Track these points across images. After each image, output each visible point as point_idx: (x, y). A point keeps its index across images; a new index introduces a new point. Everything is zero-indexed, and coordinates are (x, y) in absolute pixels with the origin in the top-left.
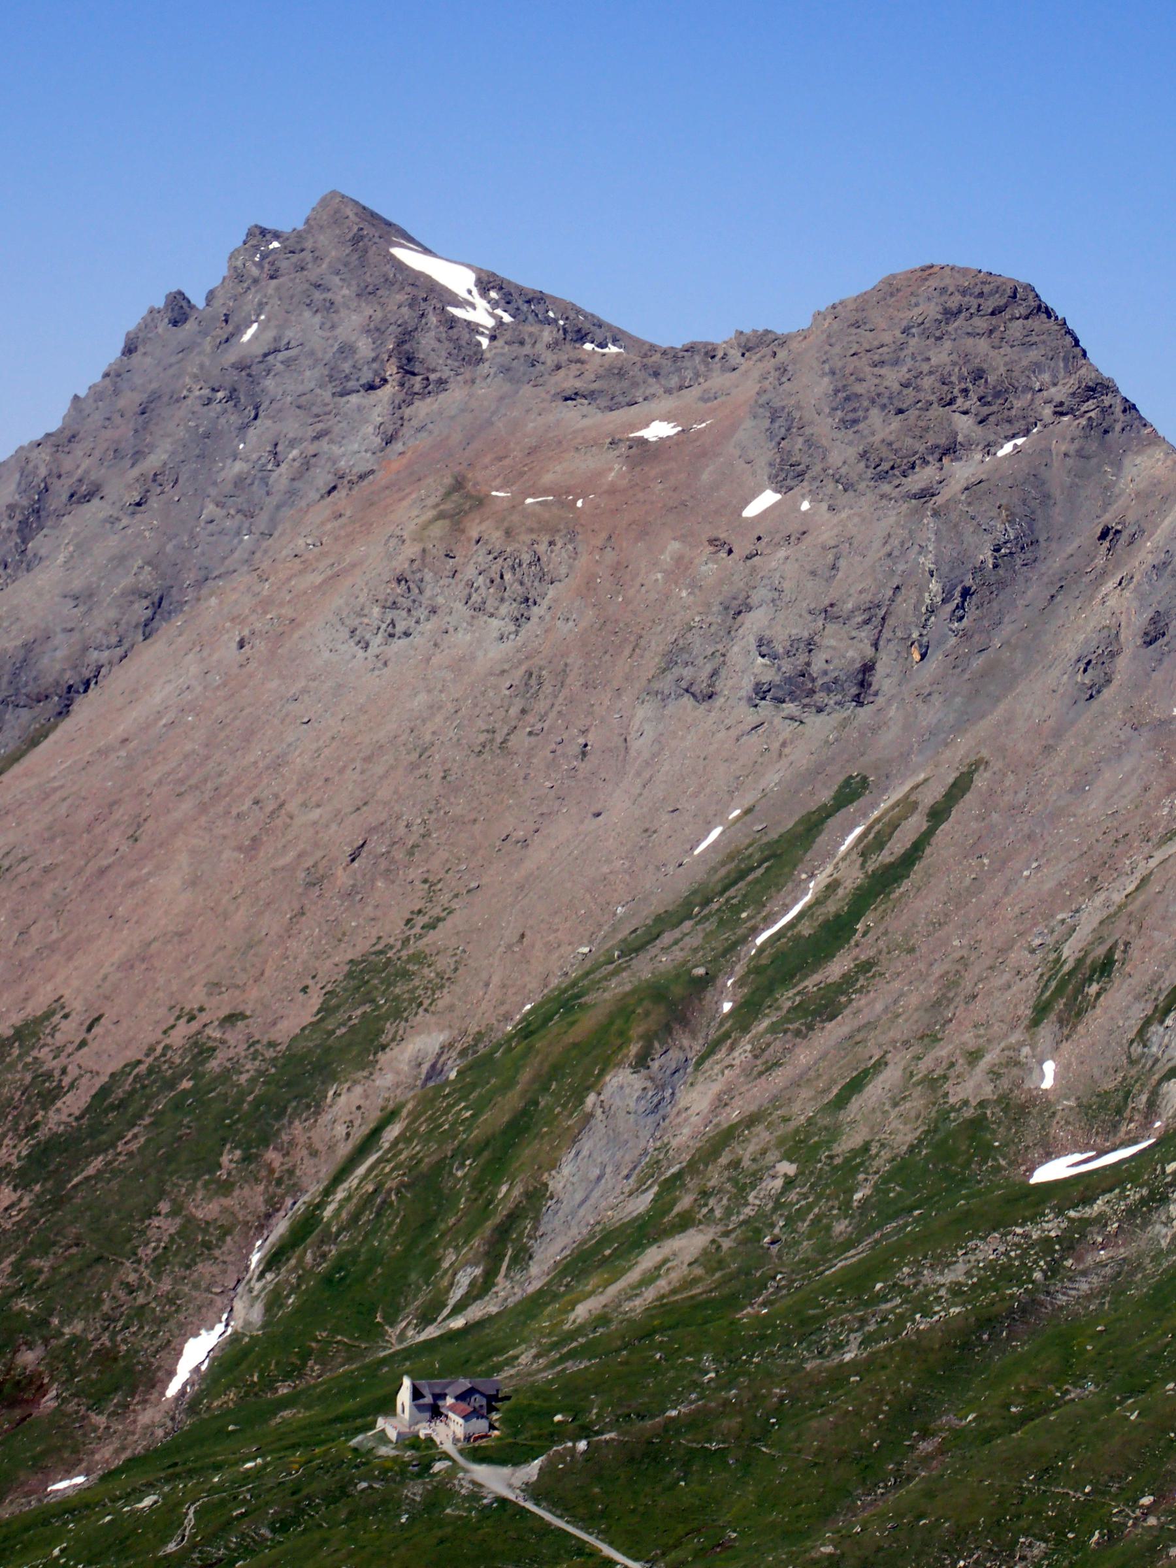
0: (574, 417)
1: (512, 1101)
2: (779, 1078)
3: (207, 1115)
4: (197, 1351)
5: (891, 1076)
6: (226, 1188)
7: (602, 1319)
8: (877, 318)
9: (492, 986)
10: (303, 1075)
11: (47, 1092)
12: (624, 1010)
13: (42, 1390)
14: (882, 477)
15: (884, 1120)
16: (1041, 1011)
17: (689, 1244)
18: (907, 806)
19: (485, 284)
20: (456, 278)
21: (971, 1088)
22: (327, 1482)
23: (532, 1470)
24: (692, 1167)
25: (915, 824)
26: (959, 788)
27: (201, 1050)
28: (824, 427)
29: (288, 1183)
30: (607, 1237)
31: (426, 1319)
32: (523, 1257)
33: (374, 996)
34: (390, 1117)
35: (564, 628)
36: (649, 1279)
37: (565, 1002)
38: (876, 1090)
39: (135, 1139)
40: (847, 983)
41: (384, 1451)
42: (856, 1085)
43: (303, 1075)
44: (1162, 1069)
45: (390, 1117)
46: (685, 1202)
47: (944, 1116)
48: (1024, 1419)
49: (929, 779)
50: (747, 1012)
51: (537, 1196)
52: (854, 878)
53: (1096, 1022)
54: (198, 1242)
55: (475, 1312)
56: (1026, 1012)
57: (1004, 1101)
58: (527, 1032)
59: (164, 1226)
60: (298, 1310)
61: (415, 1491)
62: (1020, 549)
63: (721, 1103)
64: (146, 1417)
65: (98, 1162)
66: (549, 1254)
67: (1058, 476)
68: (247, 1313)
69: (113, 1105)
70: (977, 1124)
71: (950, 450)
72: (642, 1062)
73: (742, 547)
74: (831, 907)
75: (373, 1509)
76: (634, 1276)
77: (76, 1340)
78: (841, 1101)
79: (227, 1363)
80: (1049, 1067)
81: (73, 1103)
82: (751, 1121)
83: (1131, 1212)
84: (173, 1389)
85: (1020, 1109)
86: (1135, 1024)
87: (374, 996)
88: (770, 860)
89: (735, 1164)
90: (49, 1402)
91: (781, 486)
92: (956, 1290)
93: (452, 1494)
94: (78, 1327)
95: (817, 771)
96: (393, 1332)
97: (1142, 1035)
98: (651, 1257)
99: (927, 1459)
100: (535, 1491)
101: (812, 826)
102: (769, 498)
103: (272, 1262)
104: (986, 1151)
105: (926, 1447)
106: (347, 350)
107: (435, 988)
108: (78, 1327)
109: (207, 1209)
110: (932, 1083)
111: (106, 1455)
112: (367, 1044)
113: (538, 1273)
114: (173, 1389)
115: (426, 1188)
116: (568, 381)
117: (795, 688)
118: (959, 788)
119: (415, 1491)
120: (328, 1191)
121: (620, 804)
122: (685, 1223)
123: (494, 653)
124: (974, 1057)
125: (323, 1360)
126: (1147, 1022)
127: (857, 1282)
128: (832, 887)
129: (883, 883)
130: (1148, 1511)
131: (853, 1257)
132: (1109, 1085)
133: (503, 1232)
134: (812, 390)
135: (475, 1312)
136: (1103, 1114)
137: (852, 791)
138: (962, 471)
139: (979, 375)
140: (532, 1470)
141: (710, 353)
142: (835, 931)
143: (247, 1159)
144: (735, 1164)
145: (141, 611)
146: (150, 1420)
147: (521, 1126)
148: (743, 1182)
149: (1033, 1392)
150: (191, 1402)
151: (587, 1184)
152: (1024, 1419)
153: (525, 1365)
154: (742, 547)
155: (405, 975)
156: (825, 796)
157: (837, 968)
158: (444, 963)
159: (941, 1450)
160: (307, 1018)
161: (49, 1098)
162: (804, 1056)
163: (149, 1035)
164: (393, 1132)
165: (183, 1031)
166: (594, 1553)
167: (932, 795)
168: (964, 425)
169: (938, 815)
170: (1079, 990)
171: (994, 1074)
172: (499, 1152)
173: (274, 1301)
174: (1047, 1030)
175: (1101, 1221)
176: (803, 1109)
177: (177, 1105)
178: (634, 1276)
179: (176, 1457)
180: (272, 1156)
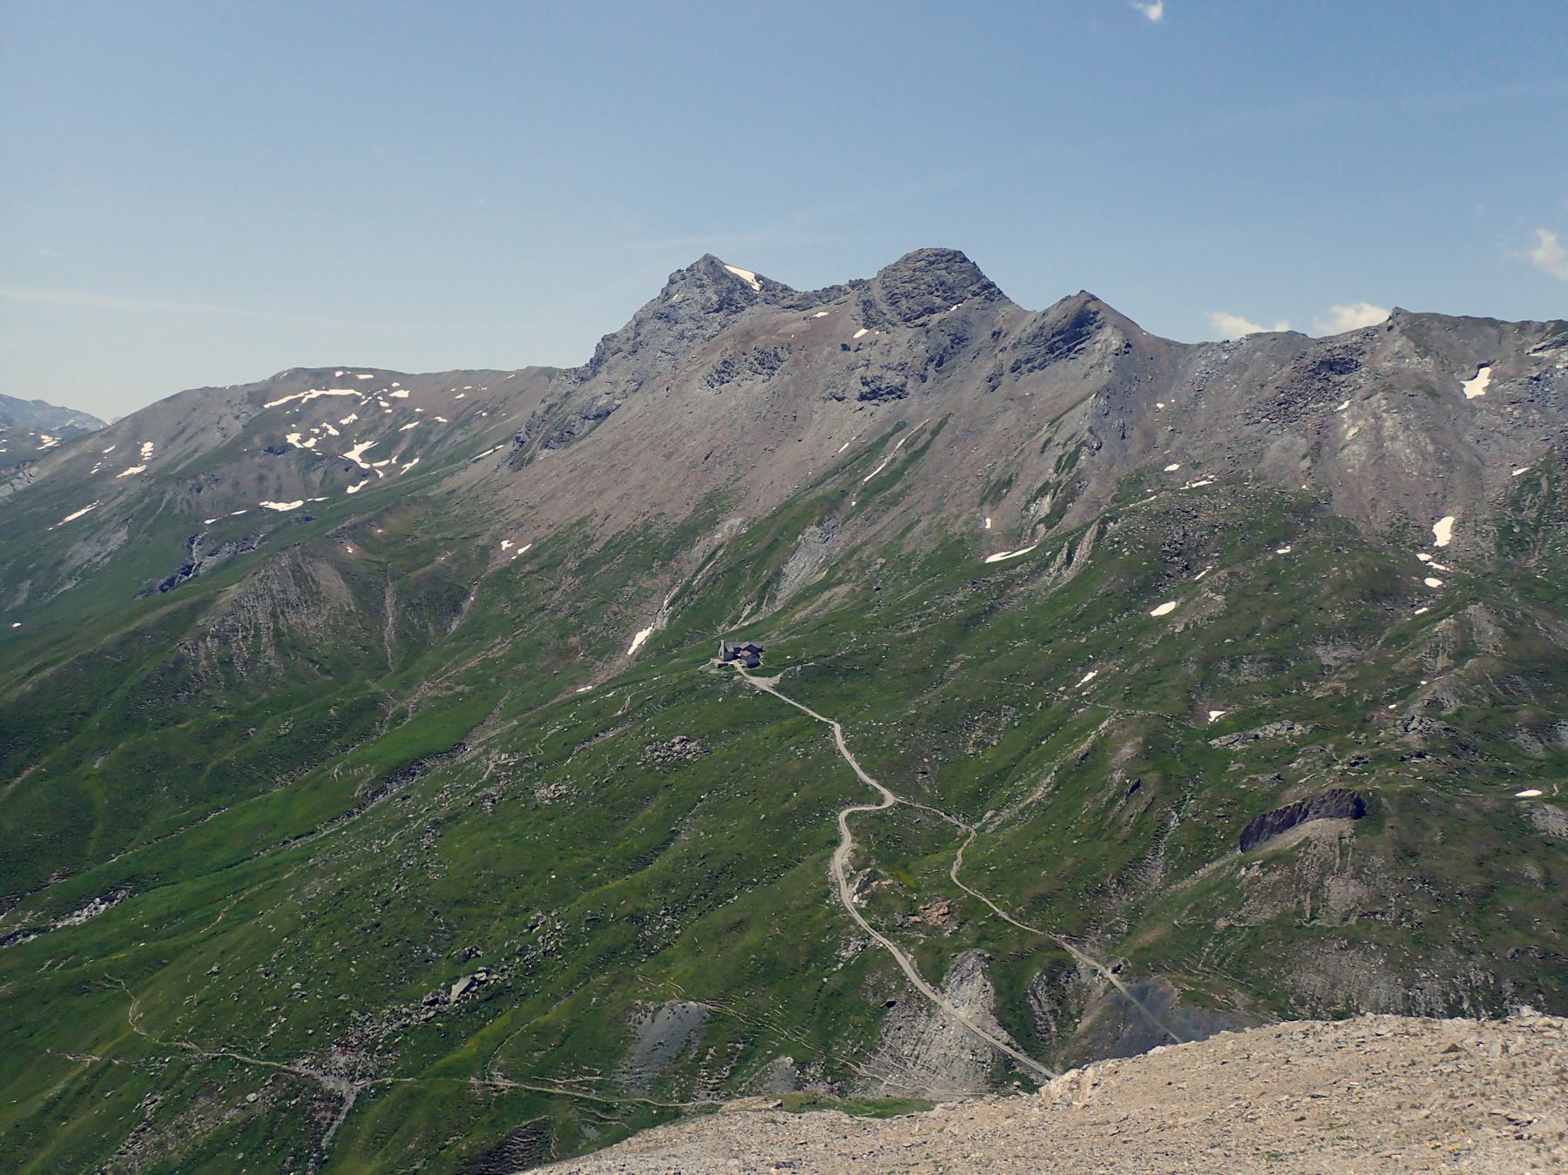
0: (789, 314)
1: (768, 539)
2: (877, 528)
3: (651, 549)
4: (641, 637)
5: (923, 525)
6: (655, 576)
7: (805, 621)
8: (902, 267)
9: (764, 500)
10: (687, 534)
11: (587, 541)
12: (812, 504)
13: (577, 653)
14: (909, 320)
15: (920, 542)
16: (984, 500)
17: (843, 589)
18: (922, 430)
19: (758, 278)
20: (748, 276)
21: (958, 528)
22: (688, 684)
23: (776, 679)
24: (842, 561)
25: (926, 436)
26: (941, 425)
27: (647, 527)
28: (884, 307)
29: (679, 573)
30: (809, 588)
31: (733, 623)
32: (773, 598)
33: (713, 508)
34: (720, 547)
35: (787, 378)
36: (826, 603)
37: (788, 504)
38: (917, 530)
39: (620, 559)
40: (902, 493)
41: (713, 672)
42: (909, 528)
43: (687, 534)
44: (1036, 519)
45: (720, 547)
46: (840, 574)
47: (947, 539)
48: (998, 654)
49: (929, 420)
50: (862, 504)
51: (778, 574)
52: (903, 456)
53: (1006, 503)
54: (644, 596)
55: (753, 620)
56: (977, 500)
57: (971, 533)
58: (774, 515)
59: (630, 590)
60: (682, 621)
61: (726, 687)
62: (959, 340)
63: (853, 538)
64: (620, 662)
65: (604, 568)
66: (786, 590)
67: (973, 317)
68: (661, 623)
69: (613, 547)
70: (961, 542)
71: (932, 311)
72: (820, 524)
73: (853, 348)
74: (894, 467)
75: (707, 696)
76: (819, 603)
77: (592, 633)
78: (903, 535)
79: (651, 641)
80: (988, 521)
81: (598, 546)
82: (865, 544)
83: (1033, 572)
84: (630, 652)
85: (979, 536)
86: (1023, 504)
87: (713, 508)
88: (868, 452)
89: (860, 560)
90: (580, 657)
91: (866, 327)
92: (960, 603)
93: (742, 689)
94: (593, 628)
95: (887, 421)
96: (720, 629)
97: (1027, 508)
98: (826, 595)
99: (953, 673)
100: (775, 687)
101: (885, 439)
102: (863, 331)
103: (671, 604)
104: (966, 551)
105: (953, 667)
106: (709, 299)
107: (738, 502)
108: (593, 628)
109: (647, 584)
110: (940, 527)
111: (602, 678)
112: (712, 523)
113: (778, 606)
114: (630, 652)
115: (734, 572)
116: (787, 302)
117: (873, 394)
118: (941, 425)
119: (726, 687)
120: (695, 575)
121: (809, 437)
122: (840, 582)
123: (761, 387)
124: (957, 517)
125: (691, 639)
126: (1028, 502)
127: (915, 603)
128: (894, 459)
129: (916, 455)
130: (1063, 693)
131: (912, 593)
132: (1015, 526)
133: (764, 588)
134: (877, 293)
135: (753, 620)
136: (1013, 538)
137: (899, 427)
138: (936, 317)
139: (942, 283)
140: (776, 679)
141: (839, 289)
142: (894, 475)
143: (663, 565)
144: (860, 560)
145: (633, 386)
146: (620, 664)
147: (771, 548)
148: (864, 566)
149: (999, 644)
150: (638, 656)
151: (800, 569)
152: (998, 654)
153: (774, 639)
154: (853, 348)
155: (726, 497)
156: (889, 429)
157: (897, 487)
158: (742, 492)
159: (962, 667)
160: (688, 513)
161: (587, 545)
162: (886, 520)
163: (628, 521)
164: (721, 552)
165: (641, 519)
166: (805, 714)
167: (931, 427)
168: (938, 301)
169: (935, 433)
170: (999, 491)
171: (966, 523)
172: (761, 558)
173: (672, 617)
174: (987, 507)
175: (1020, 576)
176: (887, 537)
177: (637, 546)
178: (819, 603)
179: (625, 680)
180: (673, 563)
